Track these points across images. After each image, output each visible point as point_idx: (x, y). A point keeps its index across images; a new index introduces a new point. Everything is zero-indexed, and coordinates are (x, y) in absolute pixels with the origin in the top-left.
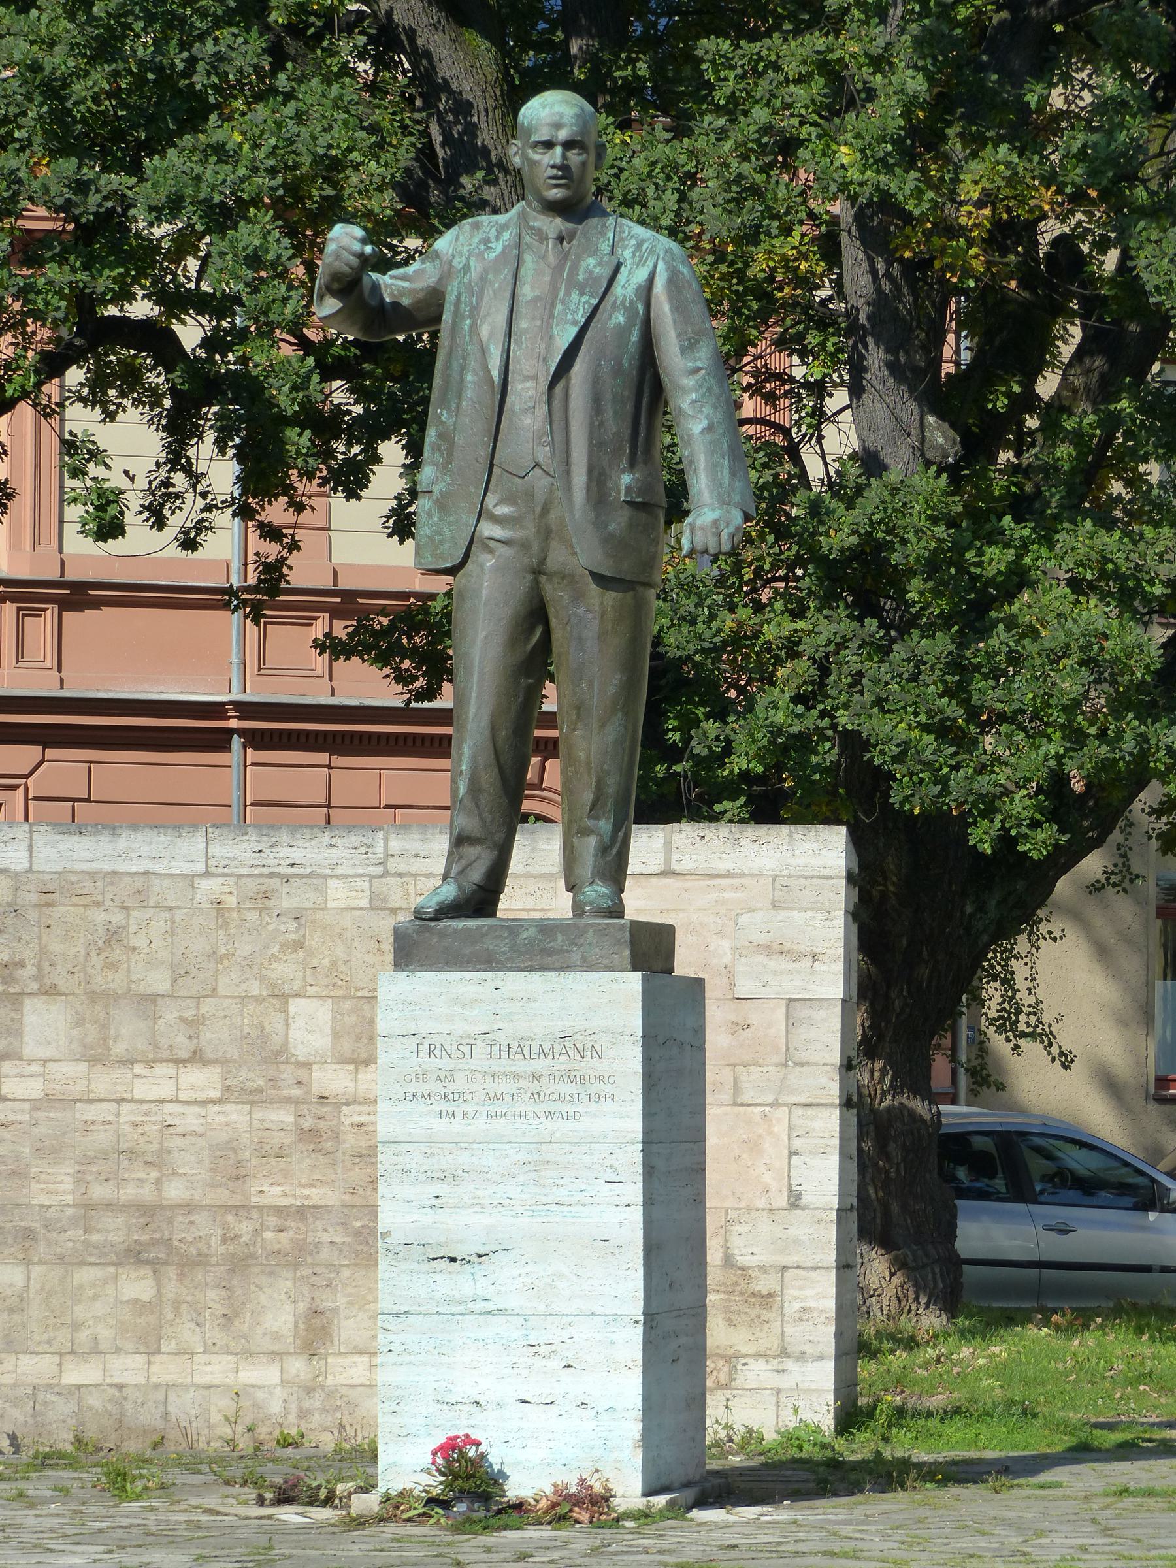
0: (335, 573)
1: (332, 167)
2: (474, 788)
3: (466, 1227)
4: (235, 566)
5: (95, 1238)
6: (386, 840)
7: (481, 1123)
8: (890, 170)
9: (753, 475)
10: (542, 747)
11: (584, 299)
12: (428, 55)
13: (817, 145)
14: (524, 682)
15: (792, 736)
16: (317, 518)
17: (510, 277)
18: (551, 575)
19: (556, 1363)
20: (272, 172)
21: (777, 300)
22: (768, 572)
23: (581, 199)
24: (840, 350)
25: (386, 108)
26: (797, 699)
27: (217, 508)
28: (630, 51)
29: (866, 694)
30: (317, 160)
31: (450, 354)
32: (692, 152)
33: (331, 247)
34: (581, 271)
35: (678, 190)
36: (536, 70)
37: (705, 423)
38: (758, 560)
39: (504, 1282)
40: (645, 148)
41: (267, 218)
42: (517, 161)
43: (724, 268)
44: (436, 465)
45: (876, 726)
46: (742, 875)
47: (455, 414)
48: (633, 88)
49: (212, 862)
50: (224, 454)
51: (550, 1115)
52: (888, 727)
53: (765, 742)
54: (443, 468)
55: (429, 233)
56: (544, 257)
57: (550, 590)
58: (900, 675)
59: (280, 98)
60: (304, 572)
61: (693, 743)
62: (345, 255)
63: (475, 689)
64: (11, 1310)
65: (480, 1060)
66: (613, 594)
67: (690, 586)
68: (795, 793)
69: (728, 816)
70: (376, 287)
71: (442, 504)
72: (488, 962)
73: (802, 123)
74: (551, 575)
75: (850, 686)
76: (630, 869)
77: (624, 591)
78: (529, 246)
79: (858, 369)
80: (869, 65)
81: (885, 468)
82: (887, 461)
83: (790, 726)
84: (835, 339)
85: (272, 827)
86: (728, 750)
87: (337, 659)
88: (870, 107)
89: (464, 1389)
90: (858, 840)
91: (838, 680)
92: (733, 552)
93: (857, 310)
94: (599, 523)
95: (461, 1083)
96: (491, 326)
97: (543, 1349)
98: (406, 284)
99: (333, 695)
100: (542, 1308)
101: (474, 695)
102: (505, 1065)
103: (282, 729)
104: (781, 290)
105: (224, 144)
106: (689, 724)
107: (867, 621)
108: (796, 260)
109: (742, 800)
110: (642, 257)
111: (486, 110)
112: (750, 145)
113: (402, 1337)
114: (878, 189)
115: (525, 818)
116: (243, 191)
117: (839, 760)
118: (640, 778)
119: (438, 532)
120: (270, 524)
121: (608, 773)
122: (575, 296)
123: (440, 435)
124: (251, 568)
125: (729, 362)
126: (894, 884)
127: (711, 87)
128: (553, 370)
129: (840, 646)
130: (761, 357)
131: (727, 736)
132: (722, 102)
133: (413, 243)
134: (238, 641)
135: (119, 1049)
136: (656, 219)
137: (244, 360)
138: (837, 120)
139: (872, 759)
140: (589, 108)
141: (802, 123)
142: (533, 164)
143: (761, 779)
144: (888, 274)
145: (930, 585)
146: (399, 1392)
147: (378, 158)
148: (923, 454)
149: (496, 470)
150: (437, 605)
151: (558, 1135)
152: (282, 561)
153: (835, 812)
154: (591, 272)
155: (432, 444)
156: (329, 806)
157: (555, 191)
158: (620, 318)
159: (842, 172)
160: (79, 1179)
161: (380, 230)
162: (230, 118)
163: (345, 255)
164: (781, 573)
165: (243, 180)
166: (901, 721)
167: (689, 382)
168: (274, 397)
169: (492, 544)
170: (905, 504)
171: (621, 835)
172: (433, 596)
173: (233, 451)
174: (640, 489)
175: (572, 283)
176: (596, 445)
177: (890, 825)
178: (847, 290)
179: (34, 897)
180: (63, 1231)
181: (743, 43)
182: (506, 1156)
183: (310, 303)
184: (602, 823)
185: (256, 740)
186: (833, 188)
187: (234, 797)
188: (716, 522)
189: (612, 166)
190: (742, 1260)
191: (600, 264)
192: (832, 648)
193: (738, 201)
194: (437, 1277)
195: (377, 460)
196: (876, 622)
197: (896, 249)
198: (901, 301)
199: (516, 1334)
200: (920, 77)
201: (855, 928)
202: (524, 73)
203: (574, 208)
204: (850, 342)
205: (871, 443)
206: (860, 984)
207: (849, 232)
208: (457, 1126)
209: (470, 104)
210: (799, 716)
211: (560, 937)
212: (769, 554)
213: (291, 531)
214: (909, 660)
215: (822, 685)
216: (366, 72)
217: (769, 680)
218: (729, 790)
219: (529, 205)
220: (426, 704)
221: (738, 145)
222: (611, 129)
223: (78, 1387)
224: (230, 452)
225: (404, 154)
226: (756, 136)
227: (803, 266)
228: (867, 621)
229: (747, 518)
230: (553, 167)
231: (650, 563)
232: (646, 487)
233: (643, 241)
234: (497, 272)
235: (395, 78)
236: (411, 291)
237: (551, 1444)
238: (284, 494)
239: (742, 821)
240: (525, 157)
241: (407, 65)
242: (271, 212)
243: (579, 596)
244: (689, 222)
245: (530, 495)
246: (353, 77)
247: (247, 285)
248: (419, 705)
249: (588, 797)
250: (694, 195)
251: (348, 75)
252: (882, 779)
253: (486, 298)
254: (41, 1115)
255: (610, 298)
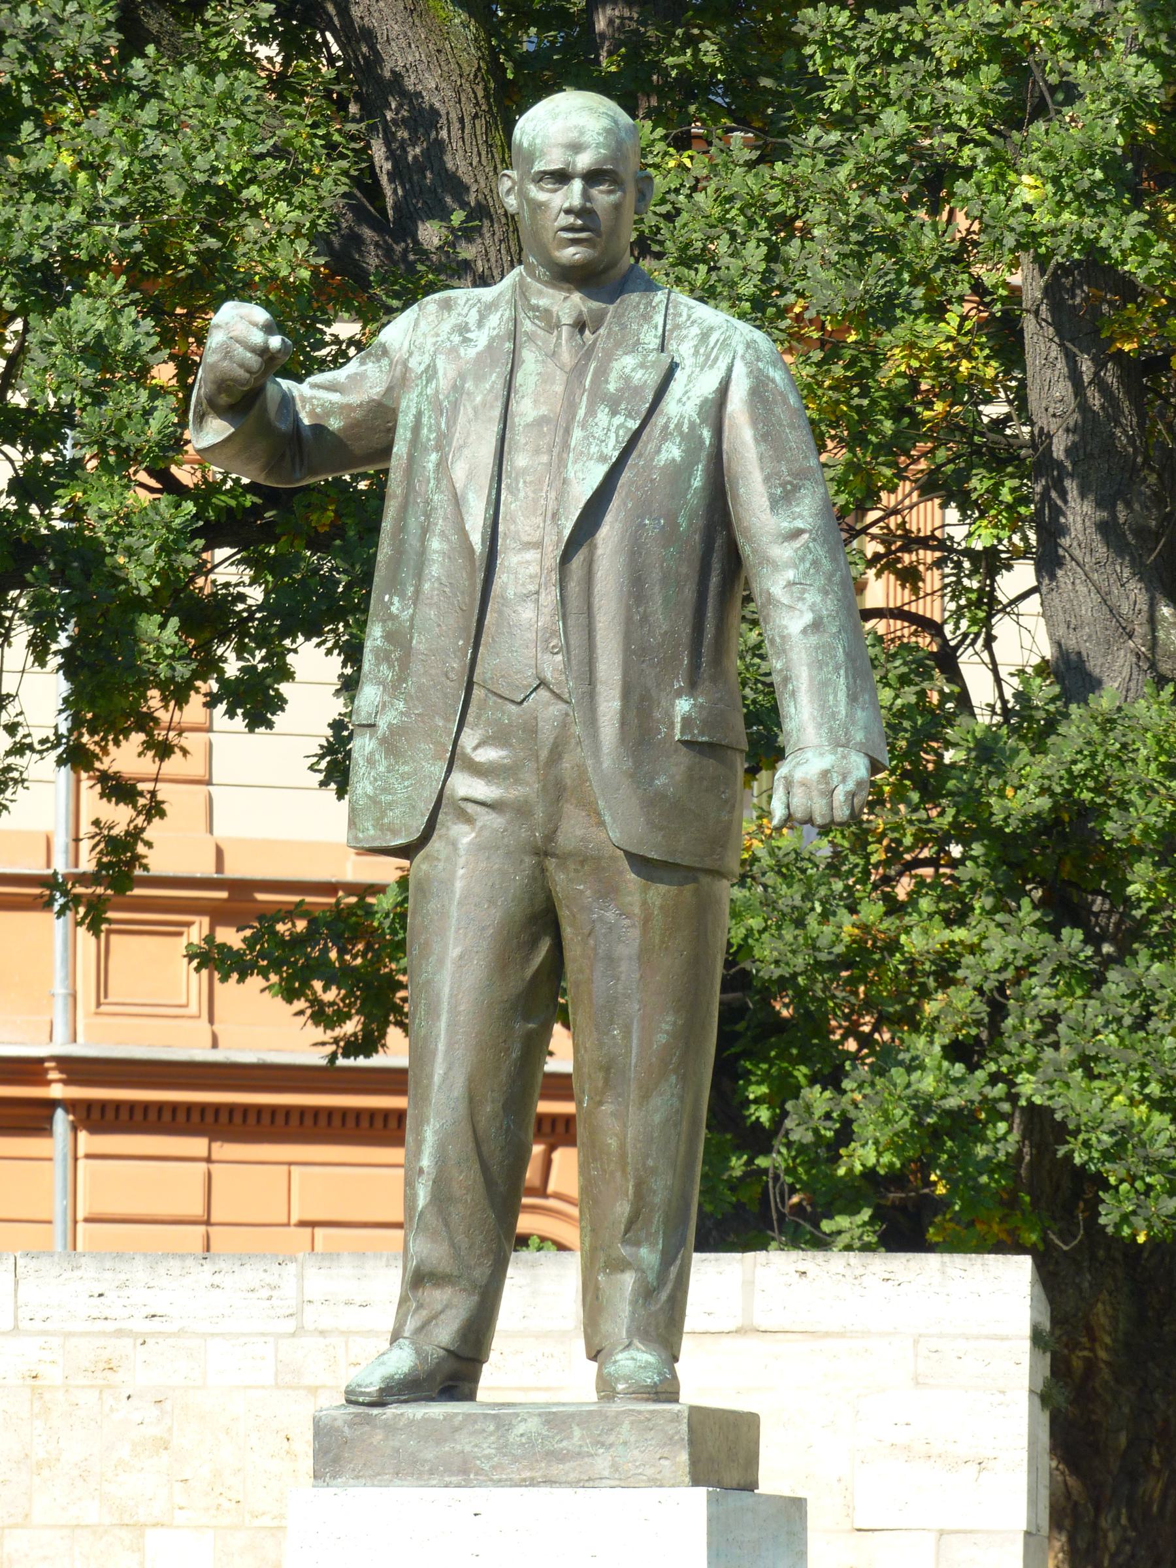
0: (219, 853)
1: (220, 205)
2: (441, 1197)
4: (61, 841)
6: (301, 1277)
8: (1100, 207)
9: (886, 695)
10: (547, 1128)
11: (618, 420)
12: (368, 35)
13: (986, 174)
14: (521, 1027)
15: (949, 1113)
16: (193, 766)
17: (500, 386)
18: (563, 858)
20: (124, 217)
21: (925, 422)
22: (909, 850)
23: (613, 264)
24: (1025, 500)
25: (302, 117)
26: (957, 1051)
27: (33, 750)
28: (688, 25)
29: (1064, 1049)
30: (195, 192)
31: (404, 508)
32: (789, 184)
33: (215, 339)
34: (613, 376)
35: (766, 241)
36: (538, 58)
37: (808, 617)
38: (893, 830)
40: (717, 176)
41: (117, 288)
42: (511, 202)
43: (838, 370)
44: (382, 683)
45: (1076, 1099)
47: (414, 603)
48: (693, 86)
49: (24, 1313)
50: (43, 664)
52: (1096, 1103)
53: (905, 1123)
54: (394, 688)
55: (374, 314)
56: (554, 354)
57: (561, 880)
58: (1119, 1020)
59: (134, 96)
60: (170, 851)
61: (789, 1123)
62: (239, 351)
63: (441, 1040)
66: (663, 888)
67: (788, 868)
68: (950, 1205)
69: (844, 1239)
70: (287, 401)
71: (391, 745)
72: (464, 1472)
73: (962, 142)
74: (563, 858)
75: (1039, 1035)
76: (688, 1326)
77: (681, 884)
78: (531, 338)
79: (1051, 531)
80: (1069, 46)
81: (1094, 684)
82: (1096, 672)
83: (944, 1097)
84: (1015, 483)
85: (119, 1256)
86: (845, 1134)
87: (225, 979)
88: (1068, 112)
90: (1051, 1278)
91: (1020, 1024)
92: (855, 817)
93: (1050, 436)
94: (640, 776)
96: (471, 464)
98: (335, 397)
99: (215, 1044)
101: (441, 1047)
103: (132, 1100)
104: (928, 405)
105: (48, 173)
106: (784, 1091)
107: (1066, 932)
108: (952, 358)
109: (866, 1214)
110: (709, 355)
111: (461, 120)
112: (880, 169)
114: (1079, 238)
115: (523, 1241)
116: (77, 246)
117: (1020, 1151)
118: (705, 1177)
119: (385, 790)
120: (117, 776)
121: (653, 1171)
122: (603, 415)
123: (389, 636)
124: (85, 846)
125: (845, 523)
126: (1107, 1348)
127: (818, 83)
128: (567, 533)
129: (1023, 973)
130: (895, 512)
131: (843, 1113)
132: (836, 107)
133: (346, 329)
134: (65, 961)
136: (733, 285)
137: (75, 512)
138: (1016, 136)
139: (1069, 1156)
140: (624, 118)
141: (962, 142)
142: (538, 207)
143: (896, 1179)
144: (1098, 381)
145: (1164, 872)
147: (292, 195)
148: (1153, 666)
149: (477, 692)
150: (384, 903)
152: (135, 835)
153: (1013, 1232)
154: (627, 379)
155: (377, 651)
156: (208, 1223)
157: (571, 250)
158: (673, 452)
159: (1024, 217)
161: (298, 318)
162: (57, 130)
163: (239, 351)
164: (925, 853)
165: (79, 228)
166: (1118, 1092)
167: (783, 552)
168: (122, 568)
169: (470, 808)
170: (1124, 746)
171: (674, 1270)
172: (377, 889)
173: (59, 660)
174: (705, 722)
175: (598, 396)
176: (635, 652)
177: (1101, 1253)
178: (1034, 404)
181: (869, 13)
183: (183, 424)
184: (644, 1251)
185: (95, 1118)
186: (1010, 240)
187: (58, 1208)
188: (825, 774)
189: (663, 201)
191: (642, 365)
192: (1010, 974)
193: (860, 257)
195: (287, 674)
196: (1079, 934)
197: (1111, 340)
198: (1118, 423)
200: (1149, 67)
201: (1044, 1418)
202: (522, 61)
203: (603, 276)
204: (1038, 489)
205: (1071, 643)
206: (1053, 1508)
207: (1037, 313)
209: (434, 113)
210: (957, 1081)
211: (577, 1432)
212: (910, 822)
213: (149, 786)
214: (1132, 996)
215: (995, 1031)
216: (270, 59)
217: (910, 1019)
218: (846, 1196)
219: (531, 272)
220: (361, 1061)
221: (859, 170)
222: (660, 147)
224: (54, 661)
225: (332, 184)
226: (888, 153)
227: (965, 366)
228: (1066, 932)
229: (875, 767)
230: (568, 212)
231: (722, 836)
232: (713, 719)
233: (711, 329)
234: (479, 378)
235: (316, 70)
236: (346, 408)
238: (140, 728)
239: (866, 1248)
240: (523, 195)
241: (335, 49)
242: (123, 279)
243: (609, 891)
244: (783, 291)
245: (531, 730)
246: (252, 70)
247: (85, 391)
248: (350, 1062)
249: (622, 1209)
250: (792, 249)
251: (243, 65)
252: (1086, 1186)
253: (462, 419)
255: (659, 421)
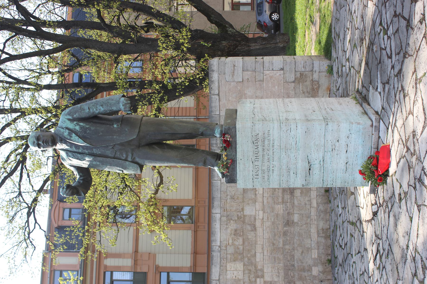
3: (301, 165)
5: (289, 201)
7: (275, 163)
19: (337, 144)
39: (316, 157)
46: (219, 80)
51: (273, 146)
64: (303, 217)
65: (259, 163)
89: (342, 166)
95: (265, 168)
97: (333, 147)
100: (323, 148)
102: (260, 157)
113: (329, 181)
135: (253, 196)
146: (343, 182)
151: (278, 144)
160: (278, 204)
169: (133, 158)
179: (225, 213)
180: (288, 207)
182: (284, 157)
190: (294, 79)
194: (314, 173)
199: (329, 154)
208: (276, 169)
223: (317, 204)
237: (358, 145)
254: (266, 211)
